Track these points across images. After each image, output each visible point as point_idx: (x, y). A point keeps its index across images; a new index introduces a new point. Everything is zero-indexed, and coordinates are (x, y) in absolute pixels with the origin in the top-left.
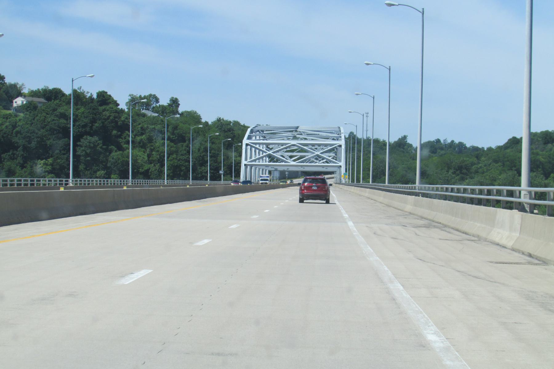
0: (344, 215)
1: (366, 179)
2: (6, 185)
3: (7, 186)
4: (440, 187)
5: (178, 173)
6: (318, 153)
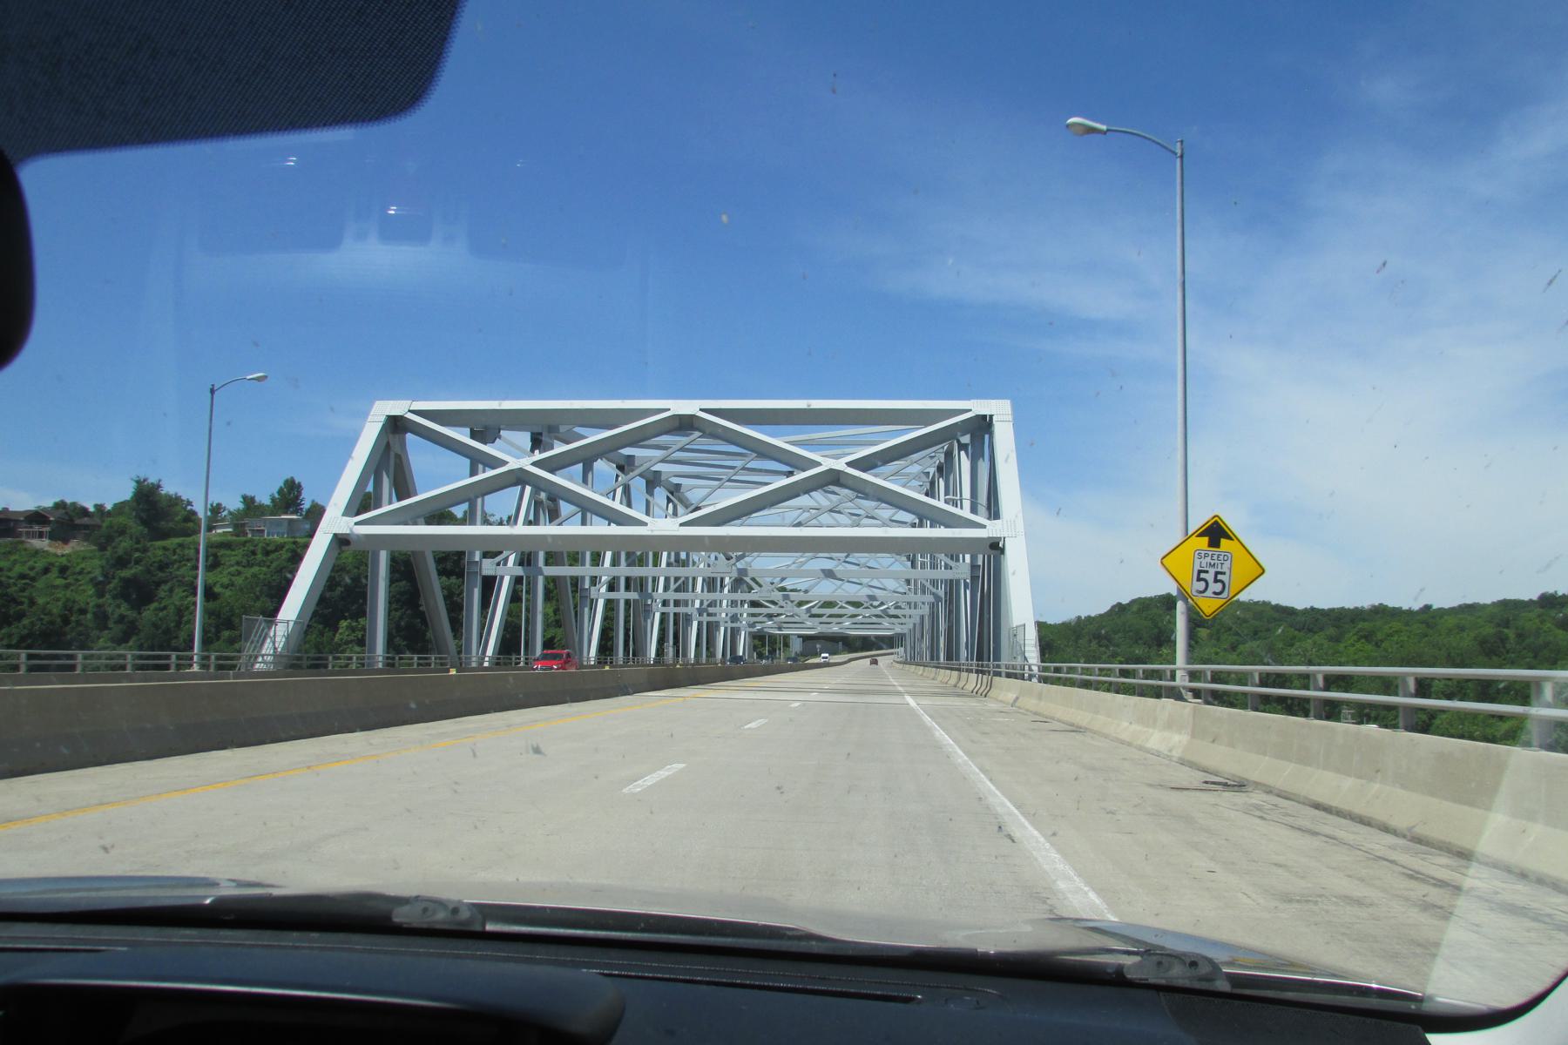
1: (934, 655)
3: (19, 671)
4: (1209, 669)
5: (346, 614)
6: (840, 465)
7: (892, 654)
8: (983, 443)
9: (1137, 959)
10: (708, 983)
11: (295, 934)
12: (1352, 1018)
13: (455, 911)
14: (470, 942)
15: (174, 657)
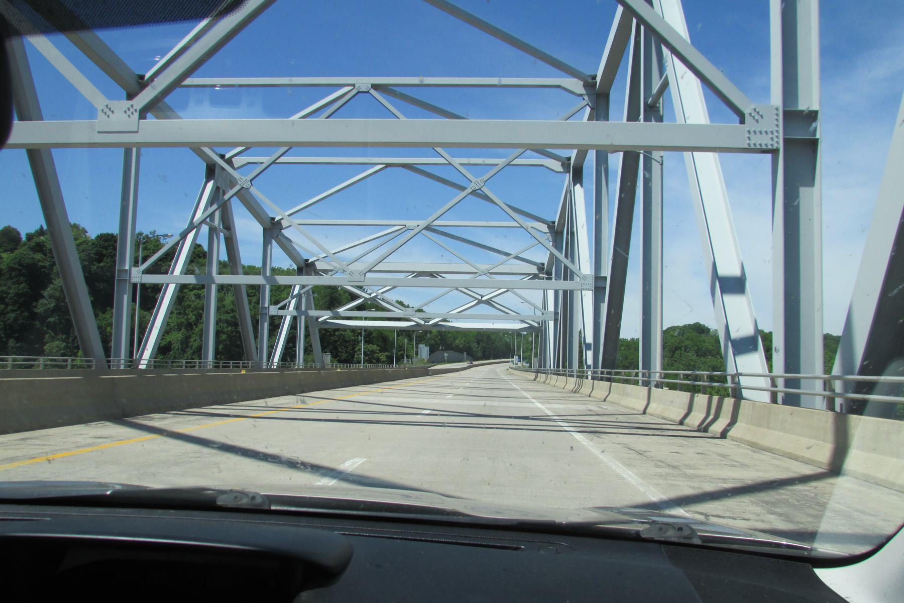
0: (330, 484)
2: (218, 367)
4: (682, 373)
7: (509, 362)
8: (563, 249)
9: (648, 526)
10: (401, 539)
11: (160, 511)
12: (772, 560)
13: (253, 498)
14: (262, 516)
15: (70, 360)
